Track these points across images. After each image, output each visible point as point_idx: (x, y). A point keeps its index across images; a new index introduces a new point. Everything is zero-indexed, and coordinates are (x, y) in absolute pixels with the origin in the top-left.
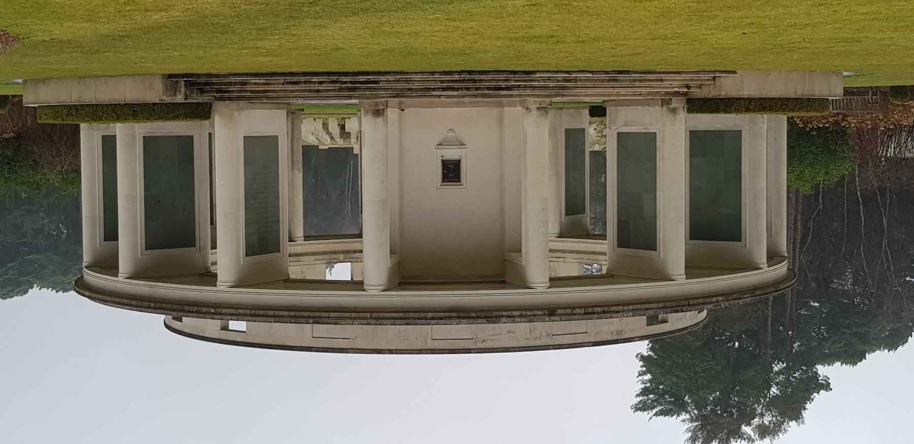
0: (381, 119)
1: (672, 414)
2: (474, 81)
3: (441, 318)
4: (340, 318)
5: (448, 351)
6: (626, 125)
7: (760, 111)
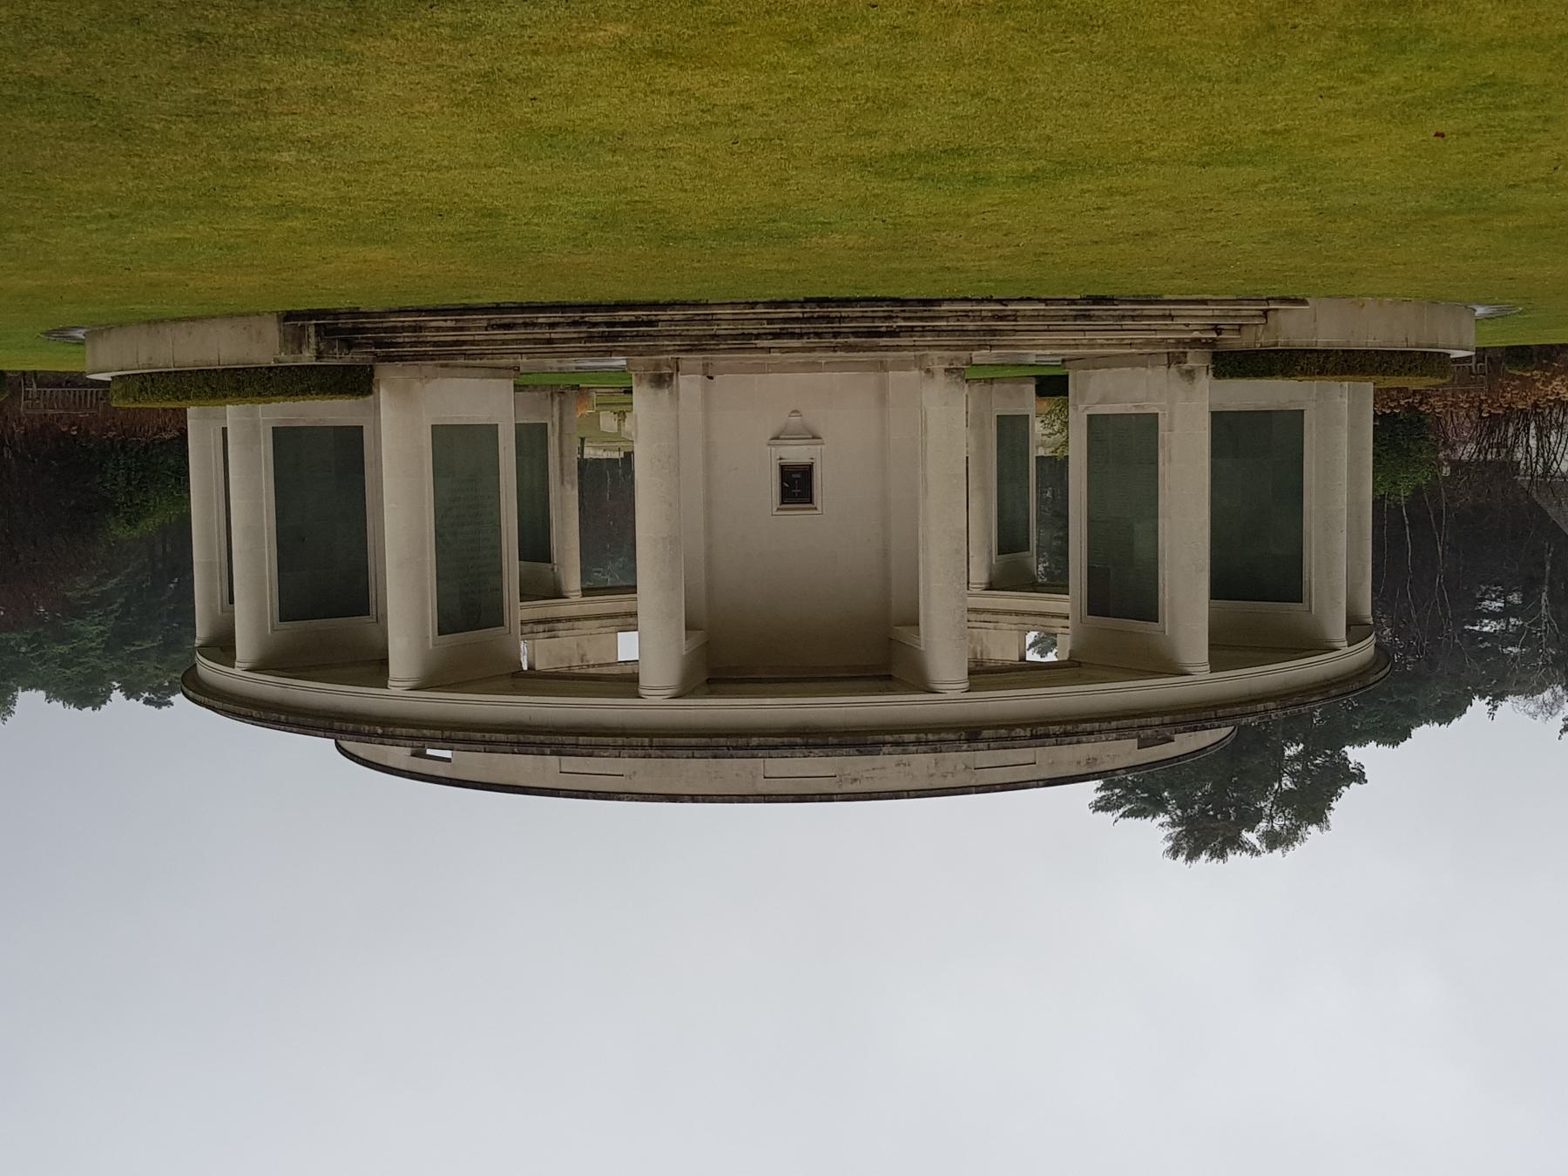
0: (667, 391)
1: (1146, 814)
2: (829, 319)
3: (776, 747)
4: (597, 746)
5: (792, 797)
6: (1103, 400)
7: (1345, 374)
